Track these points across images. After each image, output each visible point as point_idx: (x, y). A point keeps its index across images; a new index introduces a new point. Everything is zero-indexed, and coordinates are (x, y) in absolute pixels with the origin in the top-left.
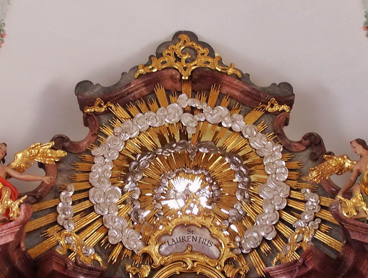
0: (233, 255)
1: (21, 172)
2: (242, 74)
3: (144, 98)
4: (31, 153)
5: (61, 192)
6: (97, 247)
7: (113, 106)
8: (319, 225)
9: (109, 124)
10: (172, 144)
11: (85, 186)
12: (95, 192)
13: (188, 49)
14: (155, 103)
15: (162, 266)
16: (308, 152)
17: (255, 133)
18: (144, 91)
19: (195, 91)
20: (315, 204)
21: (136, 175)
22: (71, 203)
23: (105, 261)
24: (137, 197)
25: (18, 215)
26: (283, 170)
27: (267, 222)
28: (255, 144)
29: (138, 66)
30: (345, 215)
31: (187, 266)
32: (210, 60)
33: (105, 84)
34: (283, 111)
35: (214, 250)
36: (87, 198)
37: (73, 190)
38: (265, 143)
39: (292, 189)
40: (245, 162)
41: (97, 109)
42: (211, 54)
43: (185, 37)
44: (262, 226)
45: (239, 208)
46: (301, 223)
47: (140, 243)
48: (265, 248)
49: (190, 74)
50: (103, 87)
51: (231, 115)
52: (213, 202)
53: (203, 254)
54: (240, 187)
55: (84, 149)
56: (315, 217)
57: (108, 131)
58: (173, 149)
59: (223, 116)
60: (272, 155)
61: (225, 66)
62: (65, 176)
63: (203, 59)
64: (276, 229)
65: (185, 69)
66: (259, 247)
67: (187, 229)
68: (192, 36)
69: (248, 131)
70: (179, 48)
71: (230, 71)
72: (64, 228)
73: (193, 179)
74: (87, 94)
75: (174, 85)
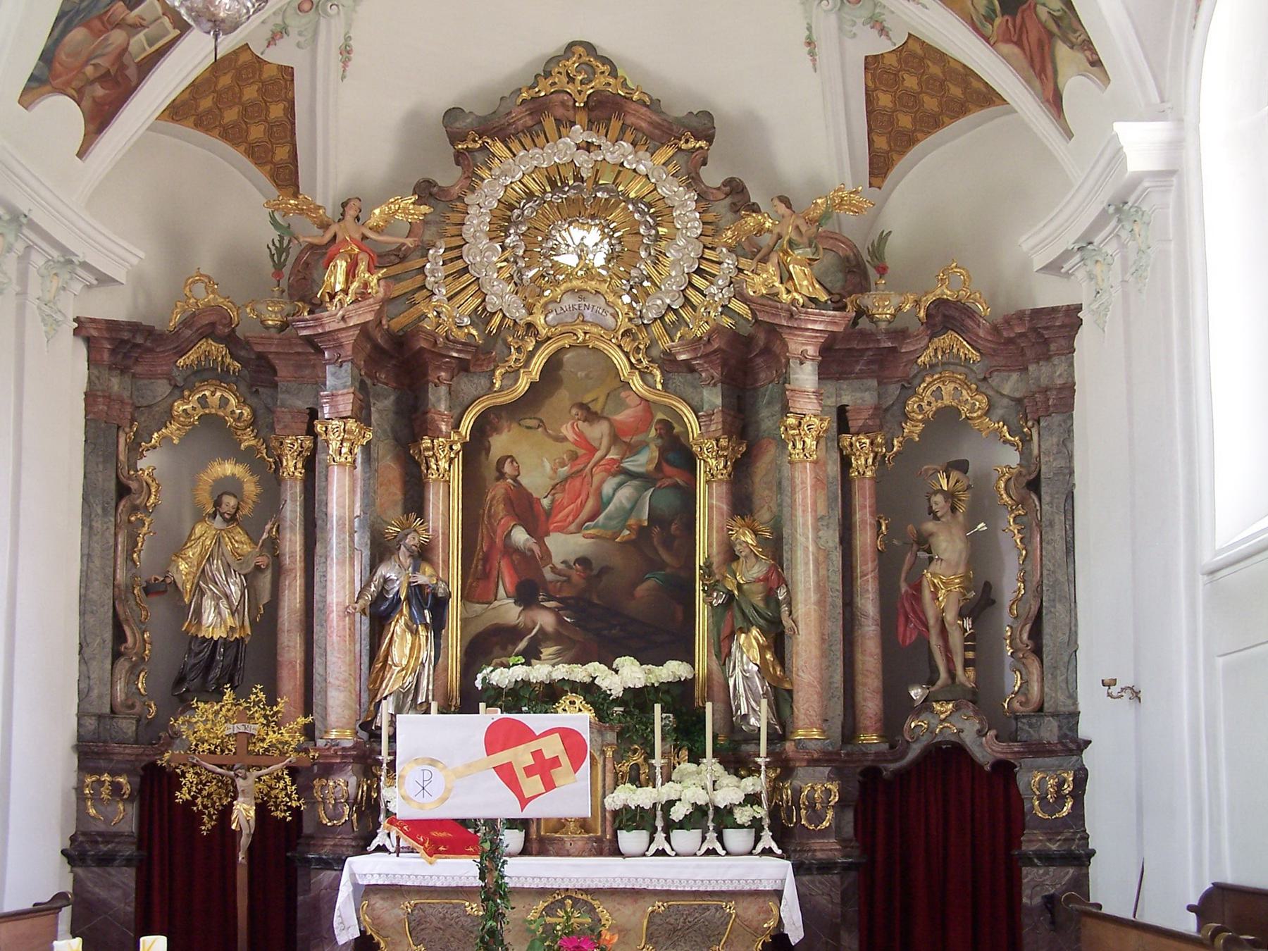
1: (378, 232)
2: (651, 99)
3: (528, 130)
4: (390, 209)
5: (429, 249)
6: (474, 316)
7: (489, 141)
10: (563, 187)
12: (469, 250)
15: (549, 338)
16: (728, 200)
17: (664, 176)
18: (529, 121)
19: (593, 121)
20: (732, 267)
21: (520, 226)
22: (441, 263)
23: (481, 332)
24: (521, 253)
27: (674, 287)
28: (663, 191)
29: (520, 89)
30: (752, 293)
31: (578, 339)
32: (611, 81)
33: (482, 111)
34: (701, 148)
35: (610, 321)
36: (461, 257)
37: (444, 247)
38: (676, 190)
39: (705, 247)
42: (613, 73)
43: (581, 50)
44: (668, 292)
45: (643, 267)
46: (714, 290)
47: (524, 311)
48: (671, 317)
49: (585, 99)
50: (477, 117)
51: (636, 152)
54: (645, 241)
55: (455, 196)
57: (484, 173)
58: (565, 193)
59: (626, 154)
60: (683, 205)
62: (433, 229)
63: (603, 80)
64: (684, 295)
66: (663, 316)
68: (590, 48)
71: (635, 97)
74: (459, 125)
75: (566, 113)
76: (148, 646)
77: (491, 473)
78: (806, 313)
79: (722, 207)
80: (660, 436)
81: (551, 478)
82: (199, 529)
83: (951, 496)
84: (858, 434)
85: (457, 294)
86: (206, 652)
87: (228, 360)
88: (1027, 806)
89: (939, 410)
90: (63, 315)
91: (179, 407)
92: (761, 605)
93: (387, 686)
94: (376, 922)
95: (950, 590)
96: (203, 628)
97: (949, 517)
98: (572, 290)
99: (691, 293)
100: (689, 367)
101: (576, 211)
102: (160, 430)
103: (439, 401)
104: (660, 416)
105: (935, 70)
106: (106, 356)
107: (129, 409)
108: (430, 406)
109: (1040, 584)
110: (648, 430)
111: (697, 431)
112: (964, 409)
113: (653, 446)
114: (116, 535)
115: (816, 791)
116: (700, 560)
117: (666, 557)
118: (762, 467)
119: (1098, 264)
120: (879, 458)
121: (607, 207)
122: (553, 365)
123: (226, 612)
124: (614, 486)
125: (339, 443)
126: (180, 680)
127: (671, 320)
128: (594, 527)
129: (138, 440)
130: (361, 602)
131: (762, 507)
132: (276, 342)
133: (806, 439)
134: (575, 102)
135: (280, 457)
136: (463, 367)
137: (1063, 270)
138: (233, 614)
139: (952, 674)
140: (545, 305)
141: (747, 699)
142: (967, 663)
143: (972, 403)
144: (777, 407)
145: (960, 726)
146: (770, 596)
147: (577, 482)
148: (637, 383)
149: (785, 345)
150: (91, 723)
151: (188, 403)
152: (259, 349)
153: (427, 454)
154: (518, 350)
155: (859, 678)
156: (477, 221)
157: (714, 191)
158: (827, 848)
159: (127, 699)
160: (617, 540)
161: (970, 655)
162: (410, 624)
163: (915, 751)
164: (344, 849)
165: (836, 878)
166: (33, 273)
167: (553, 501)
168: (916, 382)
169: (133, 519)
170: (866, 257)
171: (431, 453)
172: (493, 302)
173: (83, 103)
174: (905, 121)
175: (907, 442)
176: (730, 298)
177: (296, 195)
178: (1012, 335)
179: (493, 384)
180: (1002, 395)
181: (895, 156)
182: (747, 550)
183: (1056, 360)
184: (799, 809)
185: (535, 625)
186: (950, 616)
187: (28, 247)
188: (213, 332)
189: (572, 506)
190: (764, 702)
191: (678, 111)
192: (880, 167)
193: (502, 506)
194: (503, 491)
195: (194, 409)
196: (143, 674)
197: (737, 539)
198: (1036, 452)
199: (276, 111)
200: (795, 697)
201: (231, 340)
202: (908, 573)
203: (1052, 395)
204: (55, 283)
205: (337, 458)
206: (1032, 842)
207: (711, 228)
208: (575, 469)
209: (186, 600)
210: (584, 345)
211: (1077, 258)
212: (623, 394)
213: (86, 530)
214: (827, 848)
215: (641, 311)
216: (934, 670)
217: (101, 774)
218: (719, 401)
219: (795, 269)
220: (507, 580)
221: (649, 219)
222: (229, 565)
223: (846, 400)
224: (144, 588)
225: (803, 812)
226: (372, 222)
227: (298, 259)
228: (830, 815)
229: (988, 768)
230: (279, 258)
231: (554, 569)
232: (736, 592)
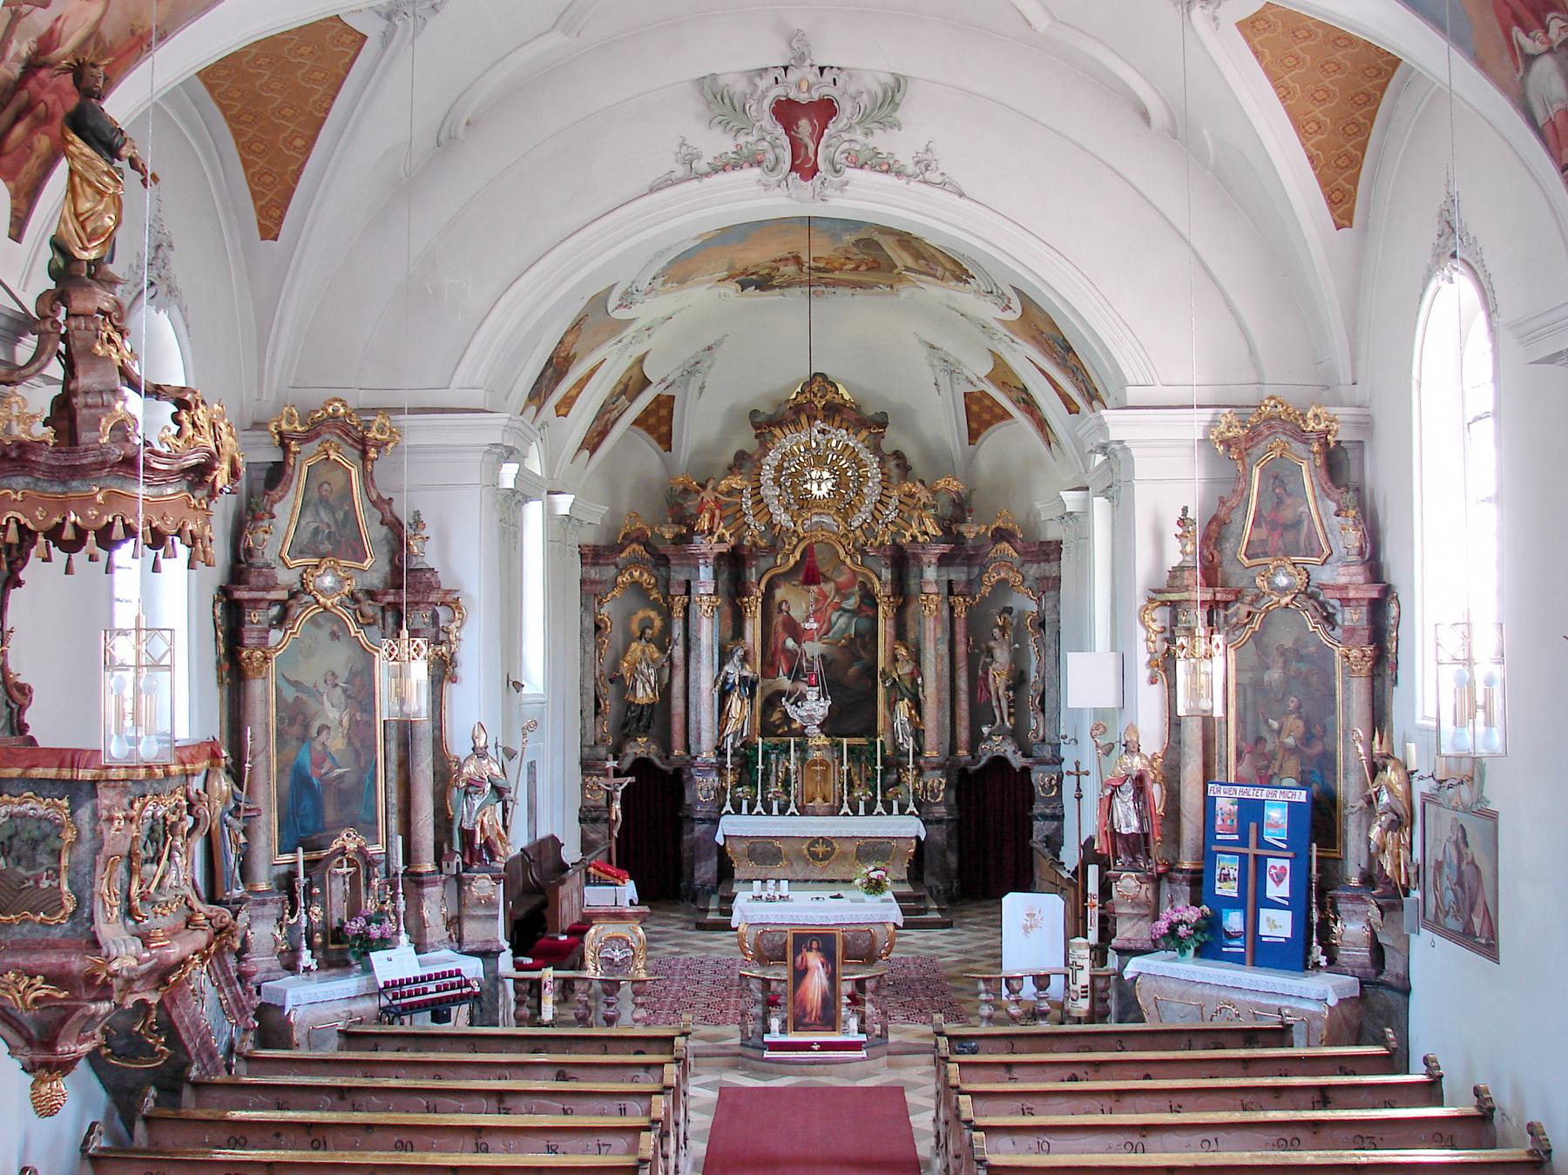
15: (804, 538)
68: (822, 375)
74: (759, 419)
82: (634, 645)
86: (639, 711)
89: (998, 581)
91: (620, 579)
92: (909, 686)
103: (752, 575)
104: (860, 579)
112: (1011, 580)
113: (857, 595)
116: (880, 669)
117: (863, 654)
118: (911, 609)
123: (649, 690)
126: (625, 725)
142: (1010, 715)
146: (914, 681)
150: (586, 750)
154: (789, 544)
156: (768, 473)
158: (940, 812)
161: (1012, 710)
163: (983, 762)
165: (944, 827)
174: (986, 417)
175: (983, 597)
183: (1052, 563)
190: (911, 738)
191: (870, 410)
192: (973, 436)
201: (647, 545)
206: (1038, 808)
210: (822, 541)
212: (842, 568)
214: (940, 812)
223: (952, 577)
228: (941, 795)
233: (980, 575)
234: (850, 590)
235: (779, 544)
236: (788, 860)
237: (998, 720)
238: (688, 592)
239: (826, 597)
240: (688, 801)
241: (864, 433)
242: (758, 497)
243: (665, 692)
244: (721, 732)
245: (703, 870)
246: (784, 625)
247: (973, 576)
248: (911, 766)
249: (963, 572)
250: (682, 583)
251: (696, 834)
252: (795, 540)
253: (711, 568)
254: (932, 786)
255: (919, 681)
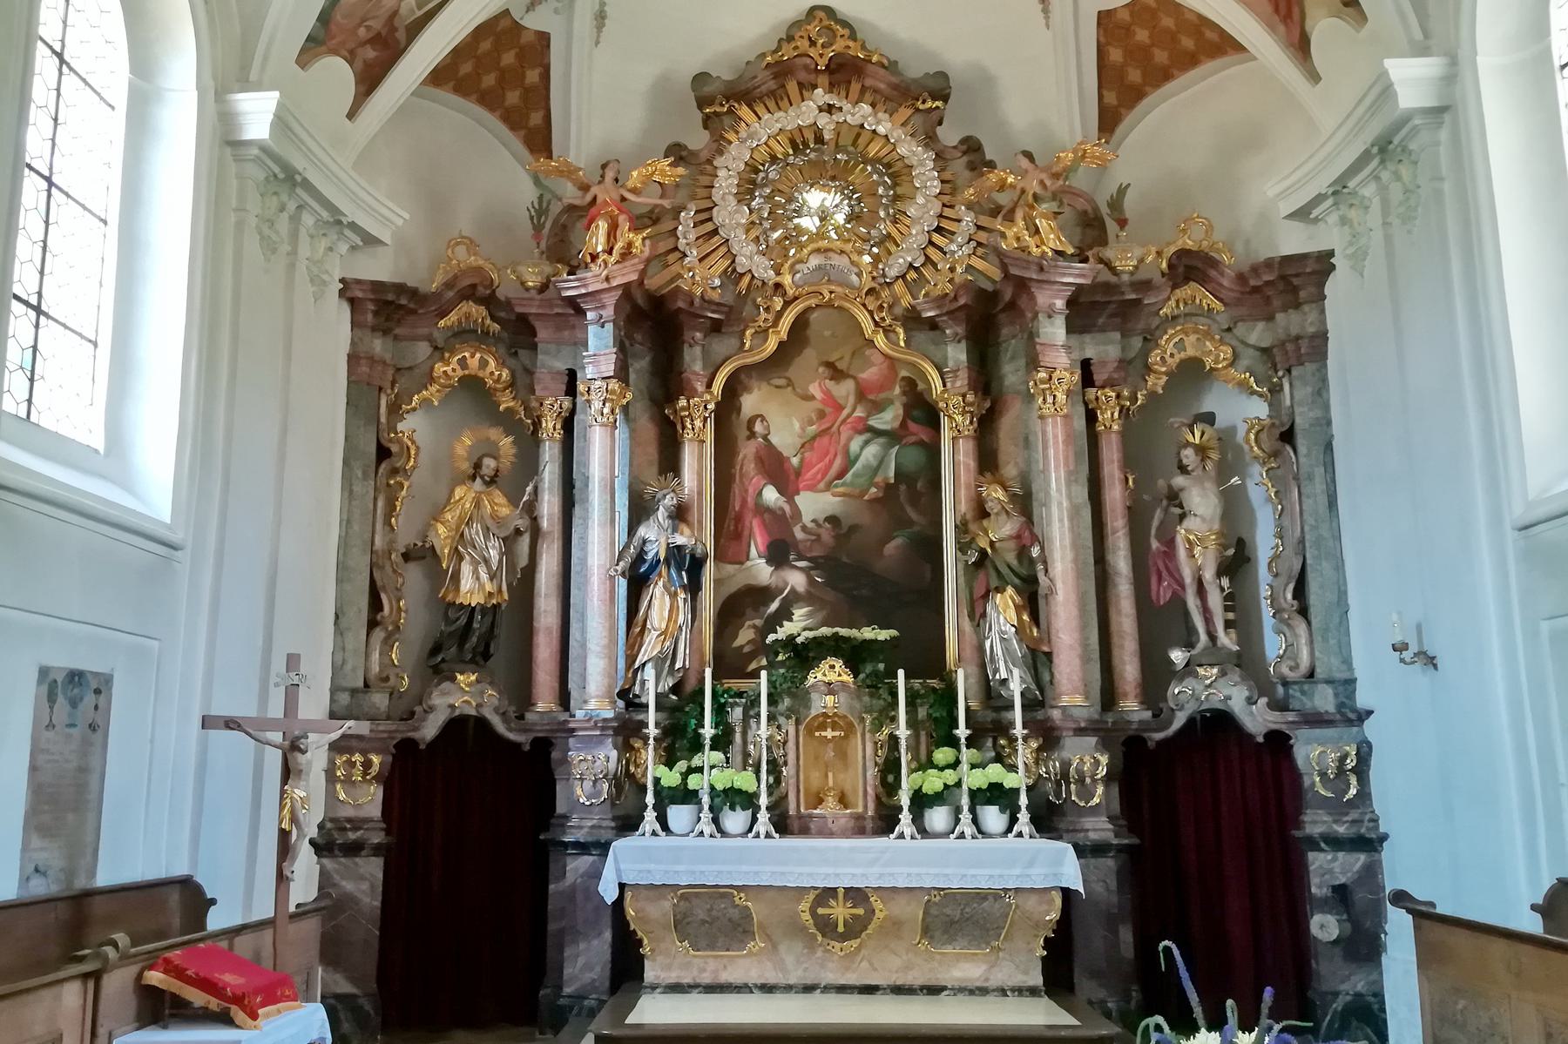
0: (876, 285)
3: (772, 94)
6: (723, 277)
7: (736, 105)
8: (975, 248)
9: (732, 127)
11: (707, 204)
13: (825, 30)
14: (786, 99)
15: (796, 298)
18: (772, 85)
25: (642, 252)
26: (936, 183)
28: (902, 150)
32: (851, 44)
34: (937, 107)
36: (710, 219)
37: (694, 209)
39: (944, 205)
40: (890, 171)
41: (718, 109)
42: (853, 36)
43: (821, 14)
46: (953, 247)
52: (852, 219)
53: (840, 285)
56: (970, 240)
57: (731, 136)
58: (807, 155)
60: (922, 163)
61: (869, 51)
65: (821, 55)
66: (905, 274)
67: (823, 255)
68: (829, 11)
69: (895, 134)
70: (813, 29)
71: (875, 59)
72: (686, 256)
73: (829, 192)
74: (708, 89)
76: (403, 614)
77: (743, 433)
78: (1056, 266)
79: (959, 166)
80: (904, 393)
81: (800, 437)
82: (459, 492)
83: (1201, 450)
84: (1103, 387)
85: (708, 255)
86: (463, 621)
87: (488, 321)
88: (1307, 782)
89: (1183, 363)
90: (331, 276)
91: (440, 368)
92: (1014, 563)
93: (646, 651)
94: (639, 915)
95: (1206, 548)
96: (461, 594)
97: (1199, 472)
98: (818, 251)
99: (931, 251)
100: (933, 325)
101: (820, 174)
102: (421, 392)
103: (694, 361)
104: (904, 373)
105: (1168, 22)
106: (370, 317)
107: (390, 372)
108: (685, 366)
109: (1302, 541)
110: (891, 388)
111: (940, 388)
112: (1209, 362)
114: (375, 499)
115: (1085, 763)
117: (912, 513)
118: (1007, 425)
119: (1354, 208)
120: (1124, 411)
121: (847, 169)
122: (800, 324)
123: (484, 576)
124: (861, 443)
125: (601, 403)
126: (436, 649)
127: (913, 276)
128: (842, 485)
129: (399, 402)
130: (621, 564)
131: (1009, 463)
132: (537, 303)
133: (1057, 393)
134: (817, 65)
135: (539, 418)
136: (716, 328)
137: (1312, 216)
138: (491, 579)
139: (1212, 637)
140: (792, 266)
141: (1006, 662)
142: (1228, 624)
143: (1216, 355)
144: (1022, 362)
145: (1227, 692)
146: (1023, 553)
147: (825, 440)
148: (880, 340)
149: (1032, 298)
151: (448, 365)
152: (519, 310)
153: (683, 414)
154: (767, 310)
155: (1115, 640)
156: (726, 182)
157: (951, 150)
158: (1099, 828)
159: (381, 671)
160: (866, 498)
161: (1231, 616)
162: (668, 586)
163: (1179, 720)
164: (603, 831)
166: (303, 233)
167: (802, 460)
168: (1158, 333)
169: (392, 482)
170: (1105, 210)
171: (687, 413)
172: (743, 263)
173: (355, 65)
174: (1134, 76)
175: (1152, 395)
176: (969, 255)
177: (550, 157)
178: (1259, 283)
179: (743, 344)
180: (1247, 345)
181: (1123, 111)
182: (999, 507)
183: (1306, 308)
184: (1068, 784)
185: (787, 584)
186: (1209, 574)
187: (300, 207)
188: (474, 294)
189: (819, 466)
191: (914, 70)
192: (1109, 121)
193: (753, 466)
194: (754, 450)
195: (454, 370)
196: (397, 644)
197: (988, 495)
198: (1288, 402)
199: (533, 76)
200: (1056, 660)
201: (490, 302)
202: (1158, 529)
203: (1304, 344)
204: (323, 244)
205: (599, 419)
206: (1315, 823)
207: (949, 188)
208: (824, 427)
209: (444, 565)
211: (1330, 202)
213: (346, 494)
215: (883, 270)
216: (1191, 630)
217: (352, 754)
218: (963, 357)
219: (1042, 224)
220: (759, 540)
221: (886, 179)
222: (488, 529)
223: (1089, 353)
224: (403, 555)
225: (1073, 787)
226: (630, 184)
227: (555, 222)
229: (1260, 739)
230: (539, 221)
231: (804, 528)
232: (989, 550)
233: (1145, 353)
234: (883, 396)
235: (748, 310)
236: (768, 938)
237: (1203, 637)
238: (571, 390)
239: (840, 408)
240: (561, 808)
241: (905, 112)
242: (709, 227)
243: (524, 585)
244: (631, 659)
245: (581, 961)
246: (759, 459)
247: (1132, 354)
248: (1019, 731)
249: (1111, 342)
250: (558, 373)
251: (570, 878)
252: (778, 303)
253: (609, 327)
254: (1079, 771)
255: (1035, 552)
